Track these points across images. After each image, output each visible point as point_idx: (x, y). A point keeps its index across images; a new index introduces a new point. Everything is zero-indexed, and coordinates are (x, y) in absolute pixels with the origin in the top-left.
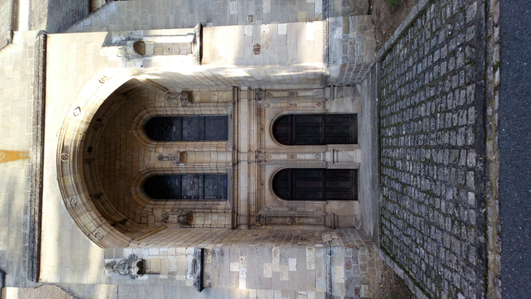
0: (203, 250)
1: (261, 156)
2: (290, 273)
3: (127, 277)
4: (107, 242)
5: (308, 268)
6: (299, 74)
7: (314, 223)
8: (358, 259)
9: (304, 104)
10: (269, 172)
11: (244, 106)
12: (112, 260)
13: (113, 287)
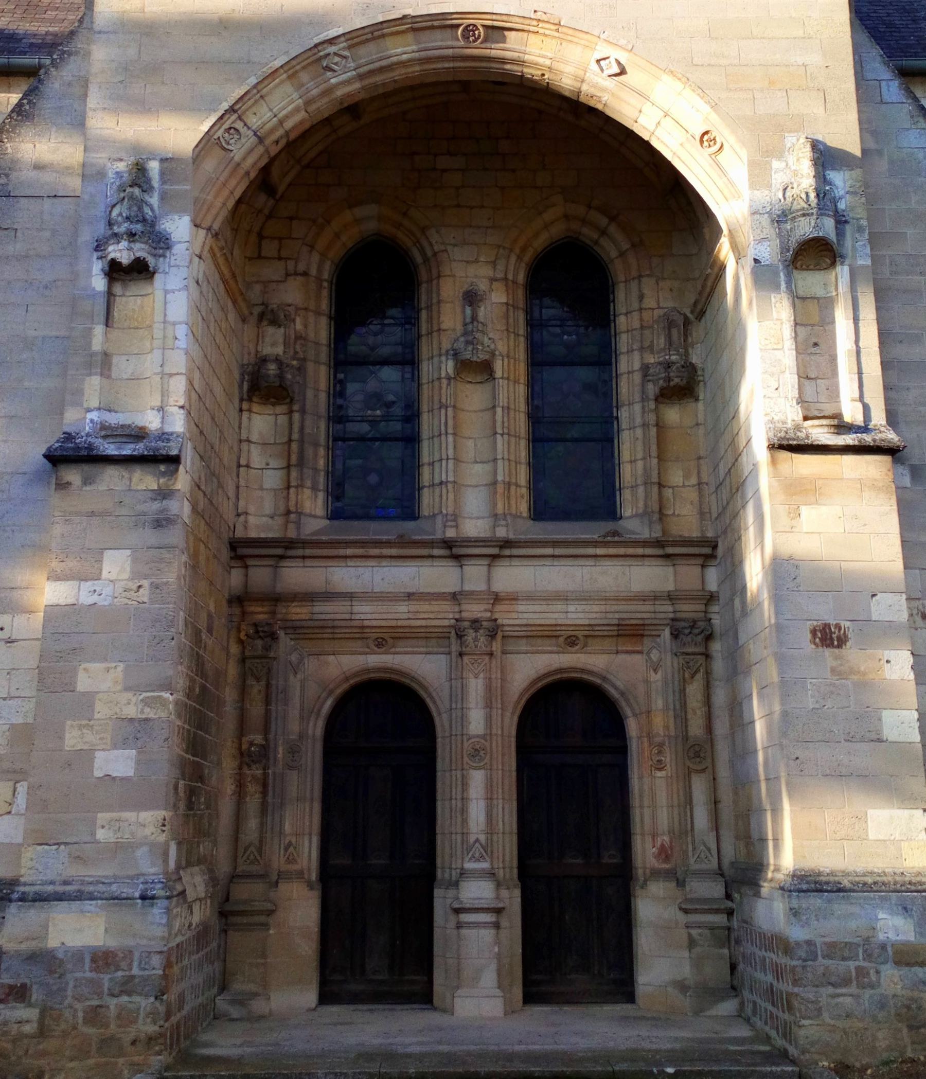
0: (175, 460)
1: (476, 640)
2: (86, 756)
3: (101, 229)
4: (209, 165)
5: (103, 817)
6: (759, 781)
7: (241, 836)
8: (125, 998)
9: (662, 798)
10: (425, 667)
11: (647, 576)
12: (156, 183)
13: (74, 184)
